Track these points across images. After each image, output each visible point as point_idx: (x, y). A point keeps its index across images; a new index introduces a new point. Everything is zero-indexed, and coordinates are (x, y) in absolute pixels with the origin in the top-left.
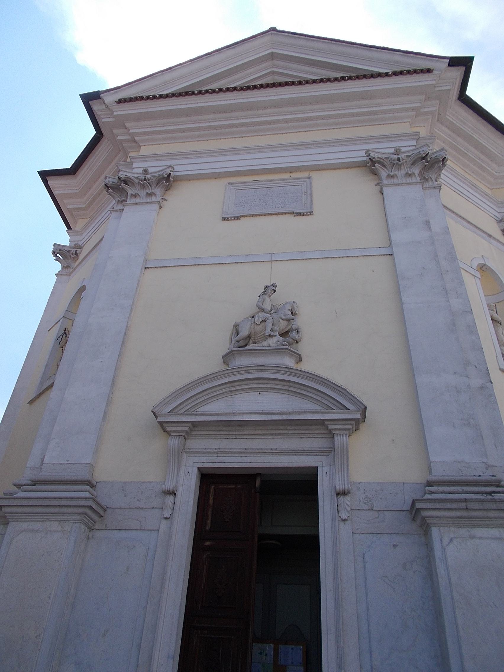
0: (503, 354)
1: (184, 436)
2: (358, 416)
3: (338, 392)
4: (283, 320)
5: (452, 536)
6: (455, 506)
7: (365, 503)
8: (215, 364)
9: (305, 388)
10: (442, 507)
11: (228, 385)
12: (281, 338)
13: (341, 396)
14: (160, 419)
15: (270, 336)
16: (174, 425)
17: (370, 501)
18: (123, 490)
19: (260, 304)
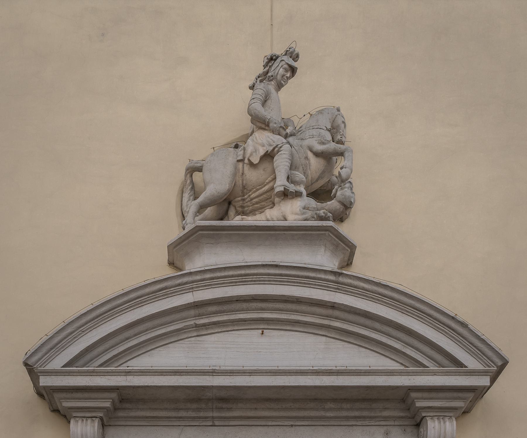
1: (101, 419)
2: (485, 381)
3: (447, 330)
4: (317, 154)
8: (154, 266)
9: (368, 322)
11: (192, 312)
12: (312, 203)
14: (45, 381)
15: (286, 195)
16: (79, 395)
19: (257, 106)
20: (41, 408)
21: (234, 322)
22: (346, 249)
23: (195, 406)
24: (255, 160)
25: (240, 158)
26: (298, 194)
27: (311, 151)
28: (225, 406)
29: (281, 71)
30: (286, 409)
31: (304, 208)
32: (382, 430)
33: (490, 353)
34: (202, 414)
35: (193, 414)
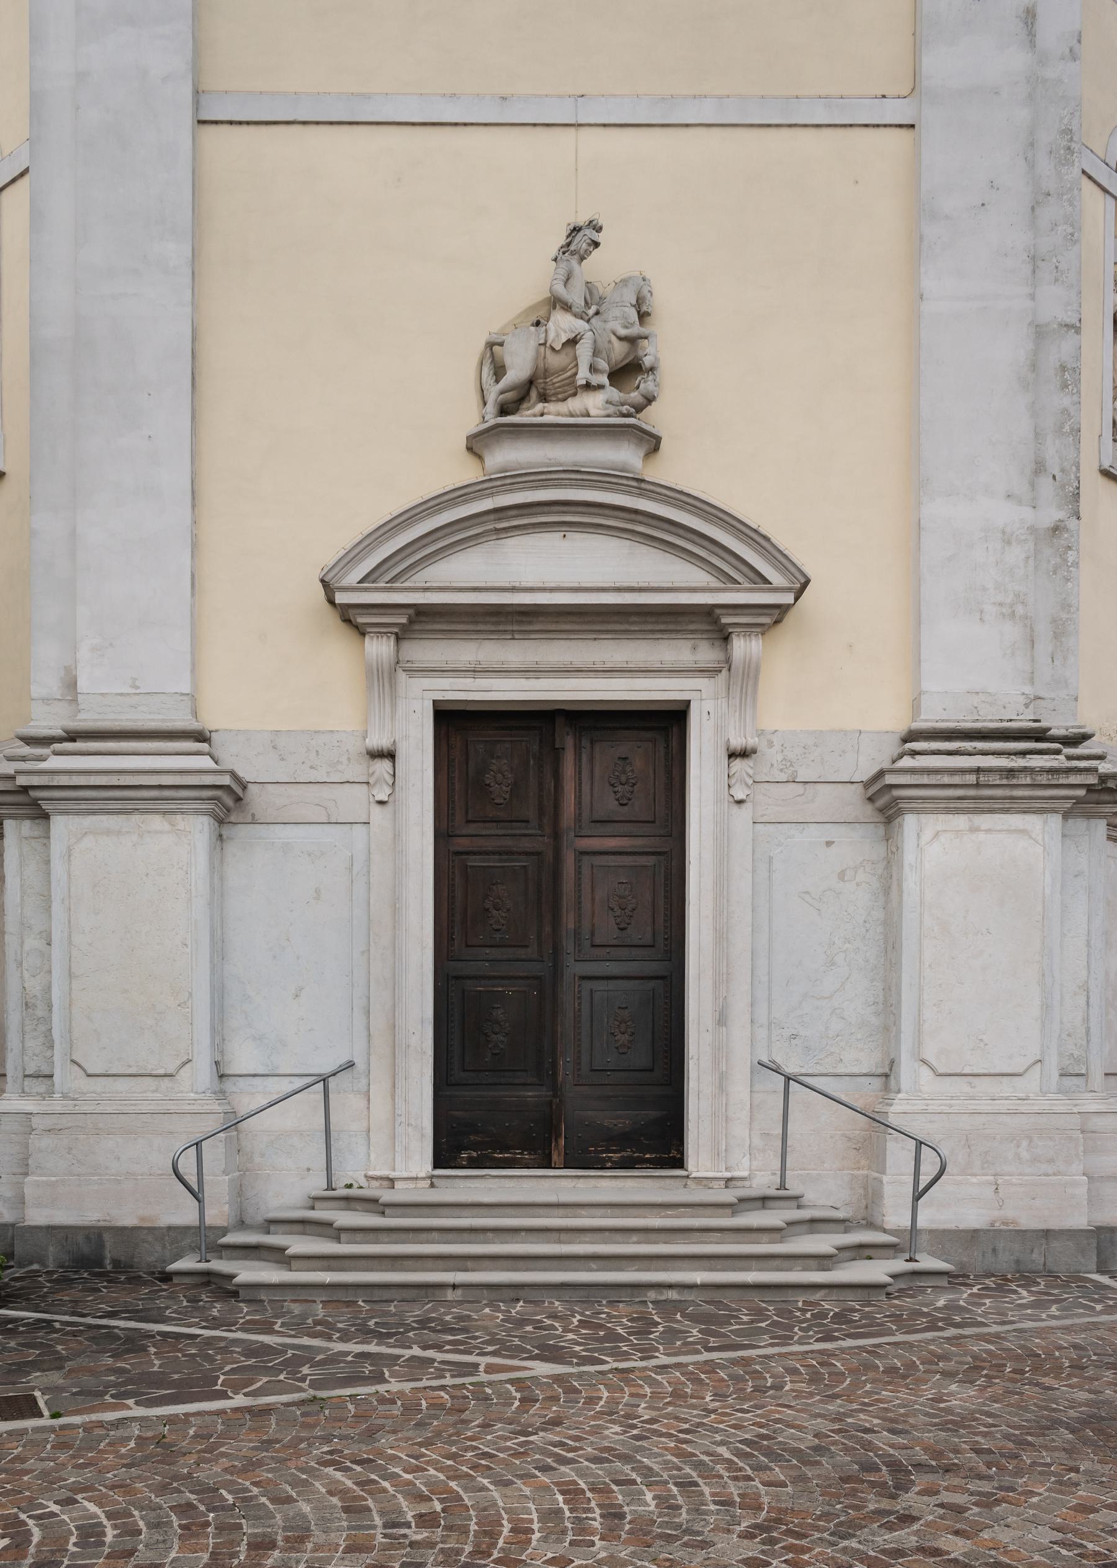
0: (1114, 422)
1: (396, 634)
2: (789, 598)
3: (750, 541)
4: (620, 339)
5: (939, 828)
6: (956, 780)
7: (781, 770)
9: (672, 528)
10: (934, 782)
11: (492, 517)
13: (755, 550)
14: (341, 598)
15: (588, 387)
17: (791, 765)
18: (274, 747)
20: (332, 618)
21: (534, 525)
22: (652, 444)
23: (494, 619)
24: (558, 347)
25: (542, 341)
26: (600, 387)
27: (614, 334)
28: (524, 619)
29: (584, 246)
30: (588, 622)
31: (607, 402)
32: (689, 644)
33: (793, 569)
34: (501, 628)
35: (493, 628)
